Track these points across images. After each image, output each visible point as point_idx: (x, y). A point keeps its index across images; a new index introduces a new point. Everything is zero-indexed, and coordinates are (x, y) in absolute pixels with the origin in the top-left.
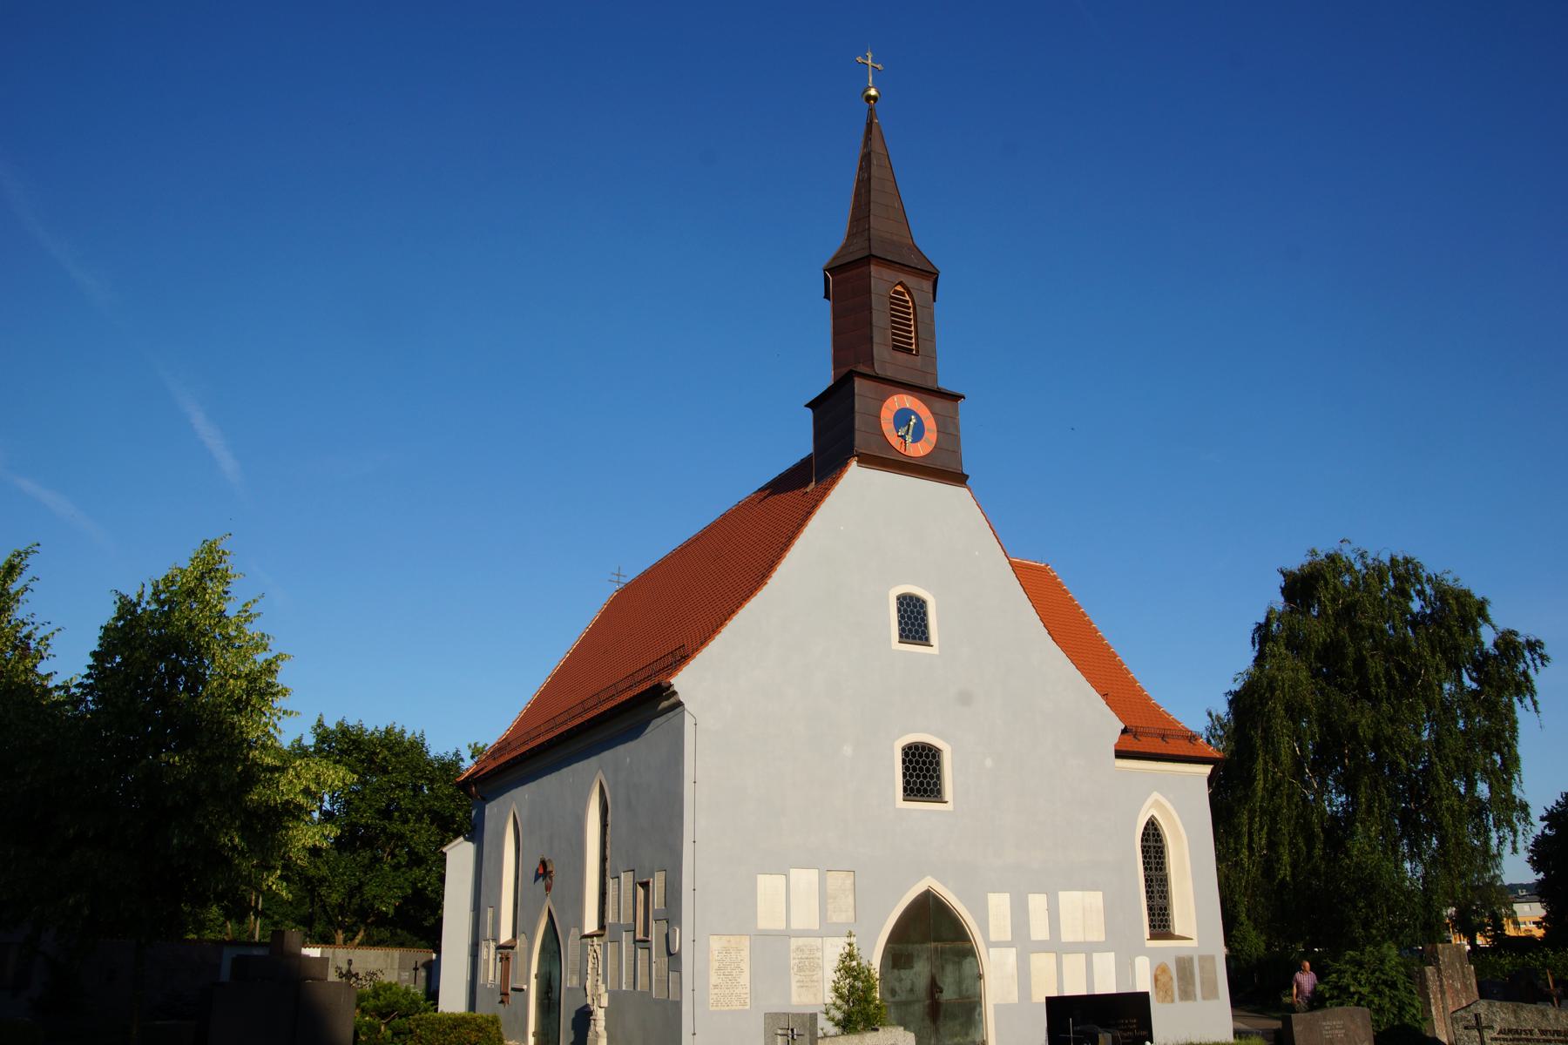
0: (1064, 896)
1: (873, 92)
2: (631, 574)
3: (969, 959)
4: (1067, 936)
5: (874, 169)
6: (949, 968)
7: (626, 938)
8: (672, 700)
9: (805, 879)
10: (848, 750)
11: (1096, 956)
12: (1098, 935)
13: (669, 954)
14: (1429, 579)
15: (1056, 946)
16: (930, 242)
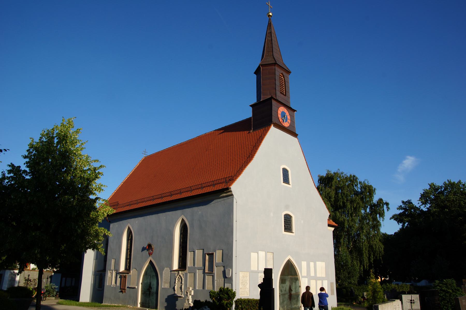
0: (317, 262)
1: (271, 14)
2: (150, 153)
6: (294, 284)
7: (199, 273)
8: (229, 193)
9: (262, 254)
10: (272, 214)
11: (324, 281)
12: (324, 275)
13: (225, 276)
14: (360, 183)
16: (287, 62)
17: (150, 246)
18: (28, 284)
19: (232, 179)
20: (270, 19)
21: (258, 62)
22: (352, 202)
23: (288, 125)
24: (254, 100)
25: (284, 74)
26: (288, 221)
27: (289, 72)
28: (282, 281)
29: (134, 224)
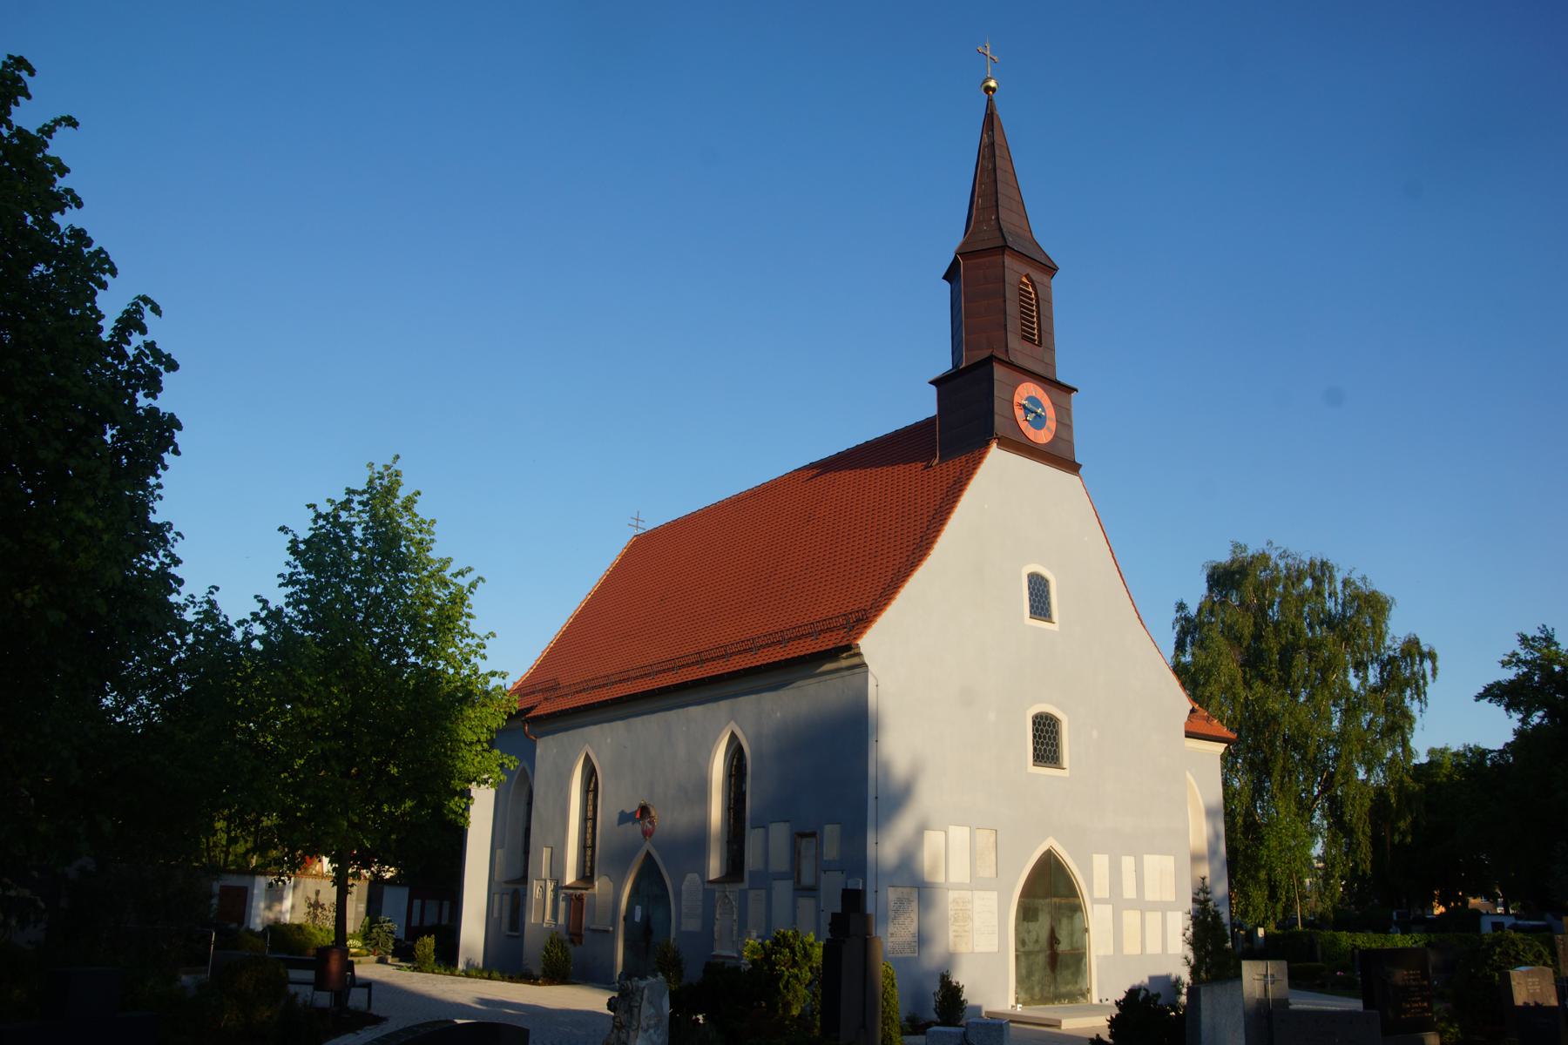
0: (1148, 859)
1: (992, 84)
2: (652, 522)
4: (1149, 896)
5: (998, 160)
6: (1065, 921)
7: (783, 889)
8: (855, 661)
9: (959, 834)
11: (1169, 914)
15: (1142, 906)
16: (1047, 233)
17: (644, 810)
18: (316, 916)
19: (864, 619)
20: (990, 100)
21: (954, 237)
22: (1313, 647)
23: (1050, 437)
24: (944, 365)
25: (1036, 276)
27: (1050, 269)
29: (601, 742)
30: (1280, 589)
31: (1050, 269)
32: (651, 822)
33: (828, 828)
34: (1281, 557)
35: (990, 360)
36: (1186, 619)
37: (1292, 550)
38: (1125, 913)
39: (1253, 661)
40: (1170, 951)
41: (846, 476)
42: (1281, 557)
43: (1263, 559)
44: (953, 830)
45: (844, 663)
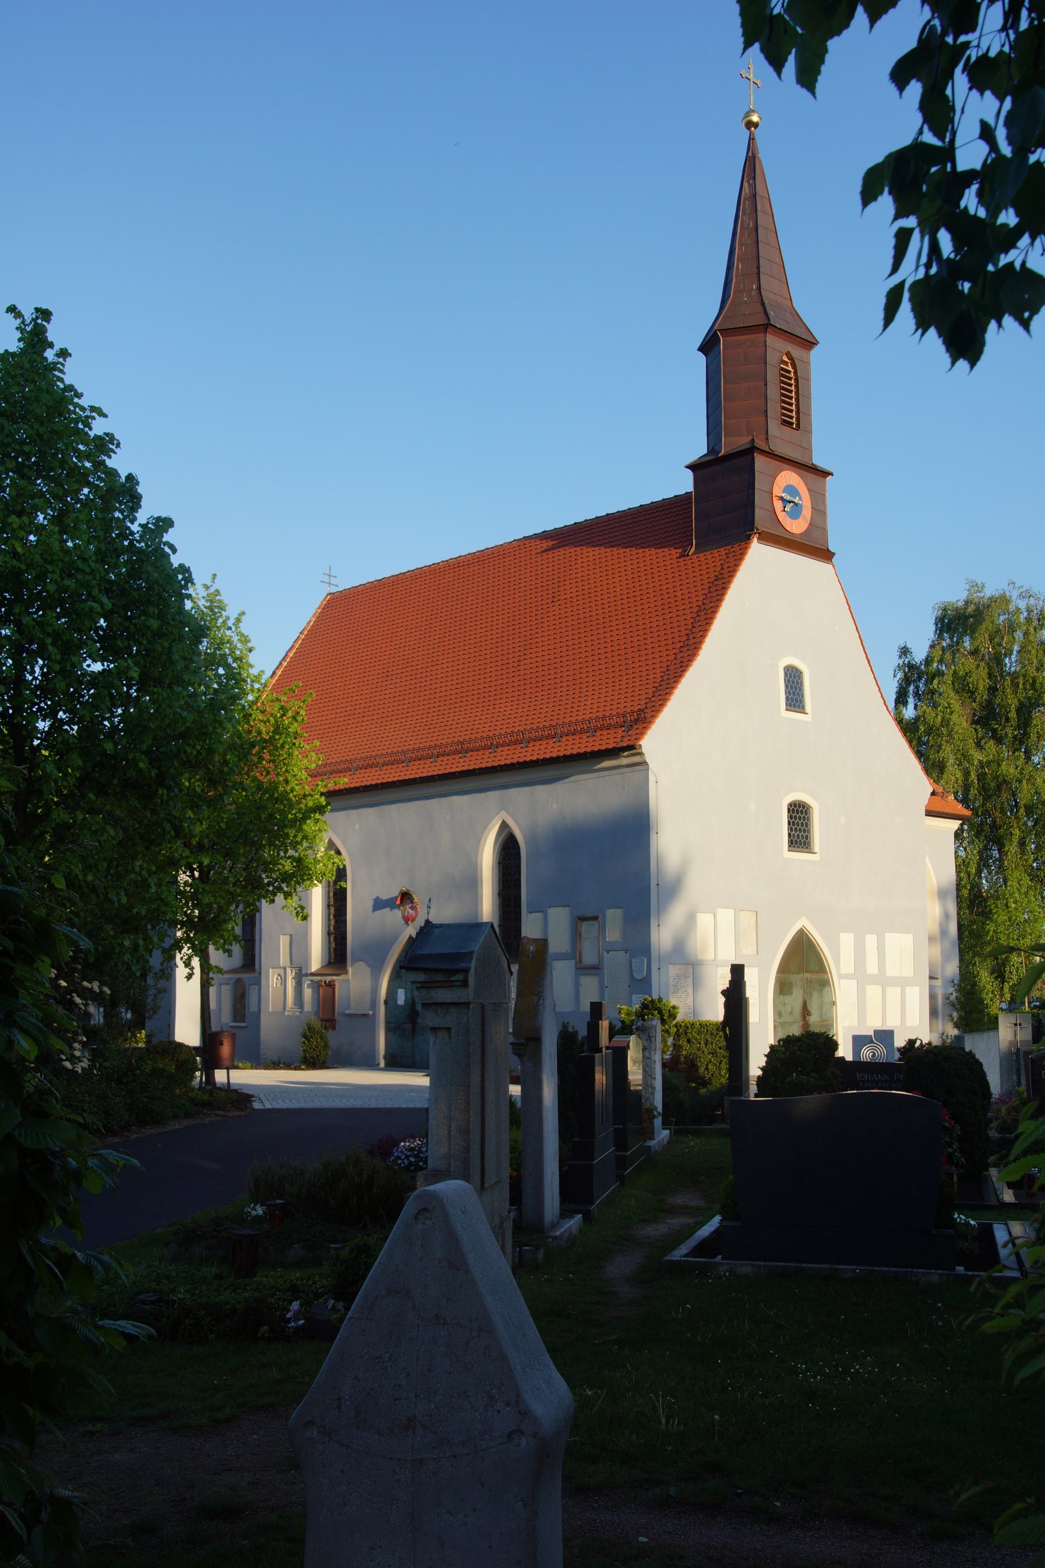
0: (889, 937)
1: (755, 118)
3: (827, 988)
4: (890, 972)
6: (815, 995)
9: (726, 916)
11: (908, 989)
15: (883, 981)
17: (406, 897)
19: (642, 719)
20: (751, 139)
24: (699, 449)
25: (796, 352)
26: (799, 816)
27: (810, 343)
28: (783, 987)
30: (1019, 635)
31: (810, 343)
32: (414, 908)
33: (610, 913)
34: (1021, 596)
35: (750, 451)
36: (911, 666)
37: (1035, 590)
38: (868, 987)
39: (987, 719)
40: (908, 1024)
41: (590, 553)
42: (1021, 596)
43: (1003, 600)
44: (720, 912)
45: (624, 761)
